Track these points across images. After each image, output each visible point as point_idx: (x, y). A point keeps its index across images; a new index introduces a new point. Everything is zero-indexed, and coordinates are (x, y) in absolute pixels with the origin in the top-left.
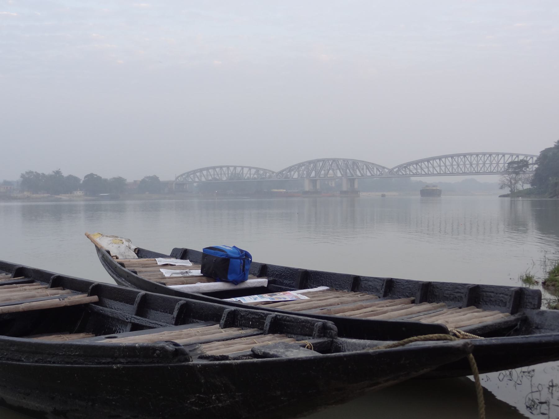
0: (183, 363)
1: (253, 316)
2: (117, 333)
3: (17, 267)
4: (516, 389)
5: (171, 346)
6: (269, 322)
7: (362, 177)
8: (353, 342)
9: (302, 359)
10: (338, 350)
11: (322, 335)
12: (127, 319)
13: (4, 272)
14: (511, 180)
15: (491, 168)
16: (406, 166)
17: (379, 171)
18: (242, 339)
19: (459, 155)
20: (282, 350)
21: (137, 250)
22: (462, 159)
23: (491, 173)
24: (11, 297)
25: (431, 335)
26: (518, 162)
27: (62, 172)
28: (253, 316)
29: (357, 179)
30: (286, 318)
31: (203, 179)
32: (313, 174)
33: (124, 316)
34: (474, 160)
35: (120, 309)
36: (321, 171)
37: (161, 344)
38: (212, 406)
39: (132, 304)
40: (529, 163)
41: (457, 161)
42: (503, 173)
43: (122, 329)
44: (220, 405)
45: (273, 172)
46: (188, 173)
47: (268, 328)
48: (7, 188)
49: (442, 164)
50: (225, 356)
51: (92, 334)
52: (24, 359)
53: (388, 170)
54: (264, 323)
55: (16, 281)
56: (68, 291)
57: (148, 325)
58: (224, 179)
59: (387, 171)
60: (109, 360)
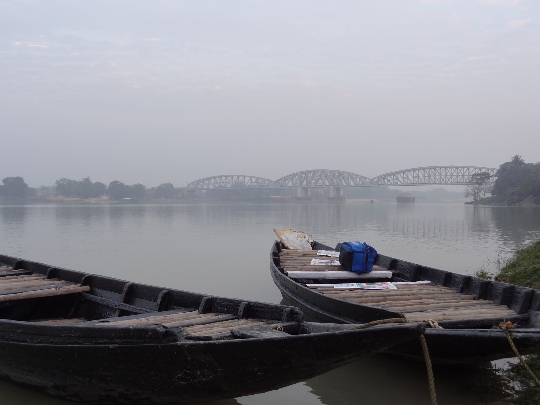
0: (173, 343)
1: (228, 303)
2: (106, 318)
3: (18, 260)
4: (308, 392)
5: (162, 328)
6: (242, 309)
7: (355, 186)
8: (318, 325)
9: (278, 339)
10: (304, 332)
11: (290, 319)
12: (116, 306)
13: (5, 265)
14: (474, 190)
15: (457, 180)
16: (384, 177)
17: (362, 181)
18: (220, 322)
19: (430, 168)
20: (257, 332)
21: (313, 243)
22: (432, 171)
23: (458, 183)
24: (13, 287)
25: (389, 319)
26: (480, 175)
27: (90, 179)
28: (228, 303)
29: (342, 188)
30: (258, 304)
31: (211, 187)
32: (305, 183)
33: (113, 304)
34: (443, 172)
35: (110, 298)
36: (312, 180)
37: (153, 327)
38: (197, 380)
39: (121, 293)
40: (490, 175)
41: (428, 173)
42: (468, 184)
43: (111, 315)
44: (204, 379)
45: (271, 181)
46: (198, 181)
47: (242, 313)
48: (44, 192)
49: (415, 175)
50: (208, 337)
51: (84, 319)
52: (29, 340)
53: (369, 180)
54: (238, 309)
55: (16, 273)
56: (63, 281)
57: (134, 311)
58: (229, 186)
59: (368, 181)
60: (105, 340)
